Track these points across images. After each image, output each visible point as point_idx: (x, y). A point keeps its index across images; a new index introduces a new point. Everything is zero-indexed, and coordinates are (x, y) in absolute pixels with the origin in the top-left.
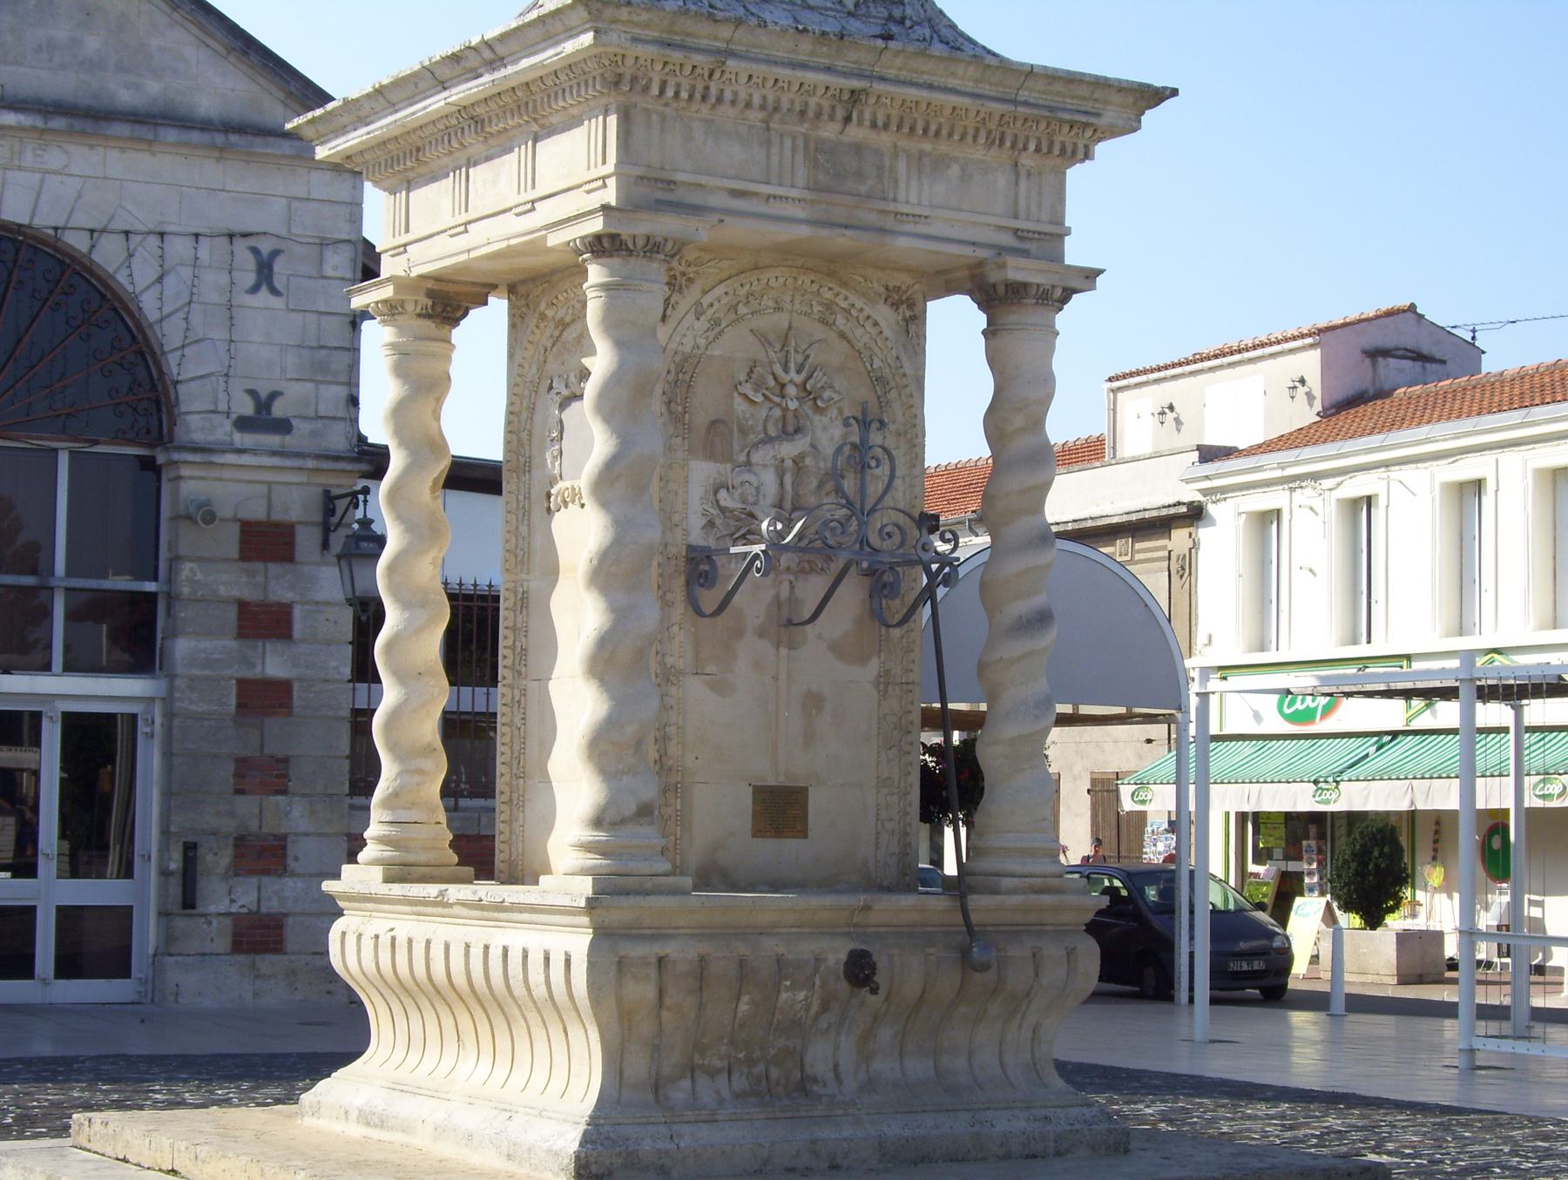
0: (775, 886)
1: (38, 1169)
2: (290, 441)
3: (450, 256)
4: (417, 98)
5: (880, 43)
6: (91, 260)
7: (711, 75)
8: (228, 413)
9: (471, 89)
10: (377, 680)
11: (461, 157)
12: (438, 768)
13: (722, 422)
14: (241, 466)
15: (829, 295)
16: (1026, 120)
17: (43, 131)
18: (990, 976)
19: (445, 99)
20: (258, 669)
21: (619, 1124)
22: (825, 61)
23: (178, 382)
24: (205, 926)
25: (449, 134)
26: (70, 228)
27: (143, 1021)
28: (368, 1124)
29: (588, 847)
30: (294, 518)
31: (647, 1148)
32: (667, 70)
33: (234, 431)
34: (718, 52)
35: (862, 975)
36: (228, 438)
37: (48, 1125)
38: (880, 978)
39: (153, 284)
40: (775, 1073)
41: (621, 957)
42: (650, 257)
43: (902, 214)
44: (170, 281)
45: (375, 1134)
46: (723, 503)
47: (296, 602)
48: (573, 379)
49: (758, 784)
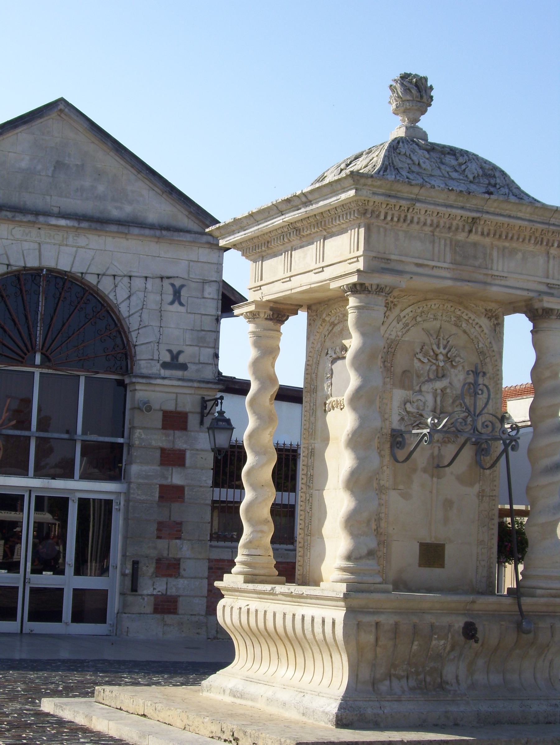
0: (429, 591)
1: (81, 712)
2: (187, 374)
3: (282, 292)
4: (269, 219)
5: (487, 196)
6: (98, 289)
7: (408, 210)
8: (158, 360)
9: (295, 215)
10: (243, 488)
11: (289, 246)
12: (269, 530)
13: (409, 371)
14: (164, 385)
15: (459, 313)
16: (553, 232)
17: (78, 228)
18: (531, 636)
19: (283, 219)
20: (169, 480)
21: (356, 701)
22: (461, 204)
23: (136, 345)
24: (141, 600)
25: (283, 235)
26: (88, 273)
27: (113, 644)
28: (234, 696)
29: (344, 569)
30: (188, 410)
31: (370, 712)
32: (388, 208)
33: (161, 368)
34: (412, 199)
35: (471, 634)
36: (158, 372)
37: (79, 691)
38: (479, 635)
39: (125, 300)
40: (428, 679)
41: (359, 622)
42: (378, 294)
43: (495, 276)
44: (133, 298)
45: (238, 701)
46: (408, 409)
47: (188, 449)
48: (338, 350)
49: (422, 542)
